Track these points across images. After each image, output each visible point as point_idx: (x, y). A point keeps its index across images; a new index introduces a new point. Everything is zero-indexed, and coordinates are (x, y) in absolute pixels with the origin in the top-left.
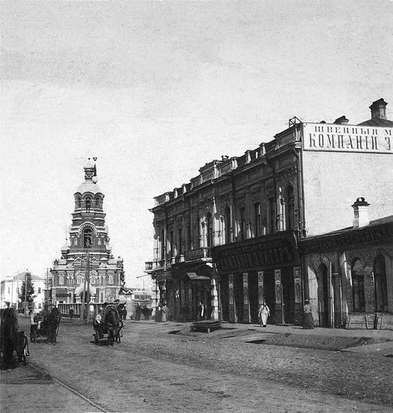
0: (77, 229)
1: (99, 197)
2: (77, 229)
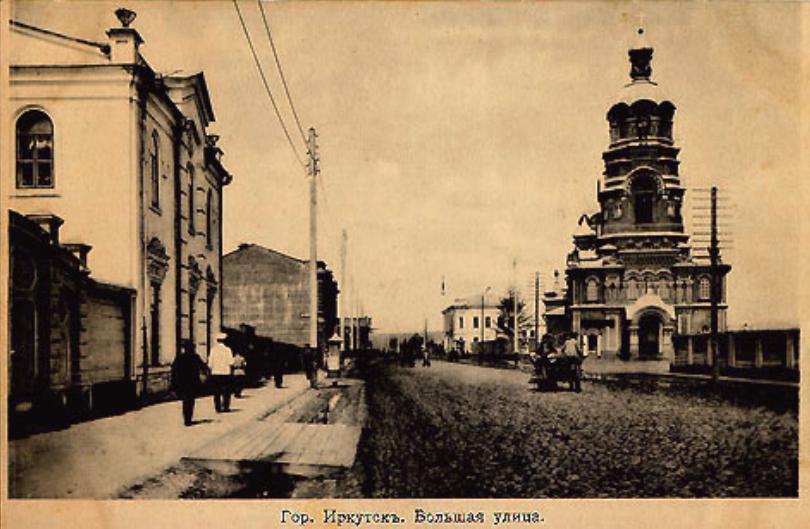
0: (619, 183)
1: (666, 111)
2: (619, 183)
